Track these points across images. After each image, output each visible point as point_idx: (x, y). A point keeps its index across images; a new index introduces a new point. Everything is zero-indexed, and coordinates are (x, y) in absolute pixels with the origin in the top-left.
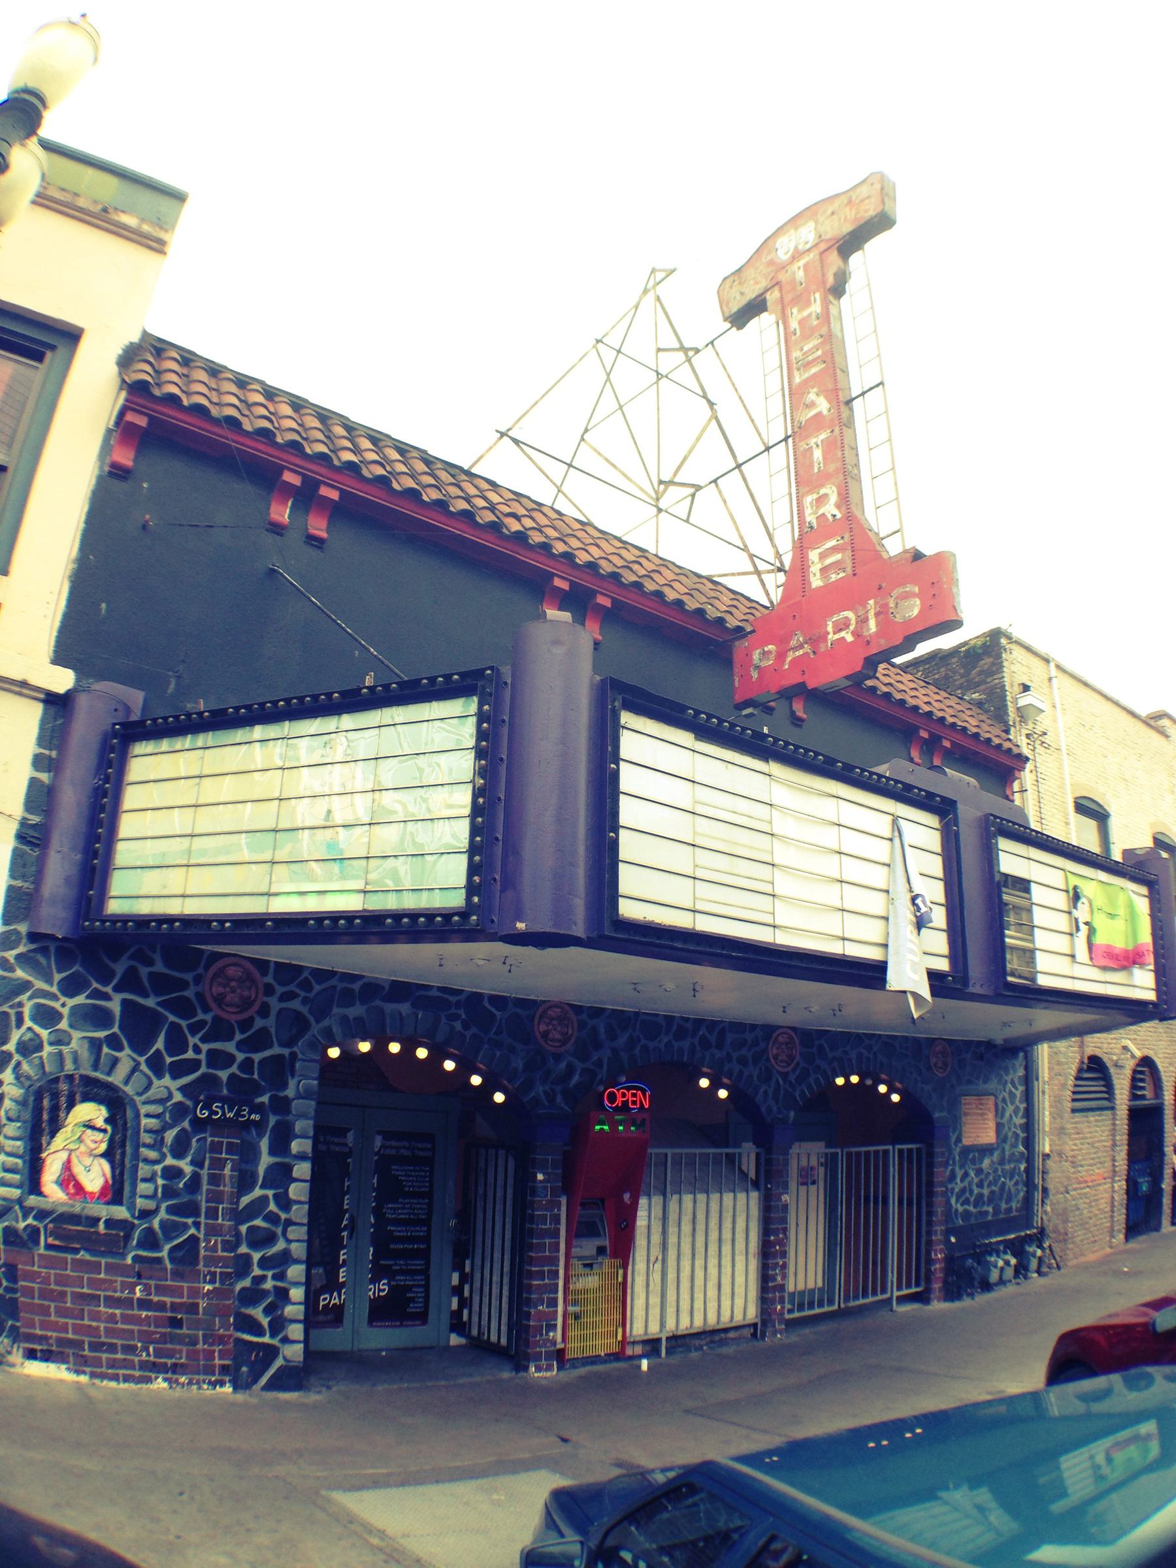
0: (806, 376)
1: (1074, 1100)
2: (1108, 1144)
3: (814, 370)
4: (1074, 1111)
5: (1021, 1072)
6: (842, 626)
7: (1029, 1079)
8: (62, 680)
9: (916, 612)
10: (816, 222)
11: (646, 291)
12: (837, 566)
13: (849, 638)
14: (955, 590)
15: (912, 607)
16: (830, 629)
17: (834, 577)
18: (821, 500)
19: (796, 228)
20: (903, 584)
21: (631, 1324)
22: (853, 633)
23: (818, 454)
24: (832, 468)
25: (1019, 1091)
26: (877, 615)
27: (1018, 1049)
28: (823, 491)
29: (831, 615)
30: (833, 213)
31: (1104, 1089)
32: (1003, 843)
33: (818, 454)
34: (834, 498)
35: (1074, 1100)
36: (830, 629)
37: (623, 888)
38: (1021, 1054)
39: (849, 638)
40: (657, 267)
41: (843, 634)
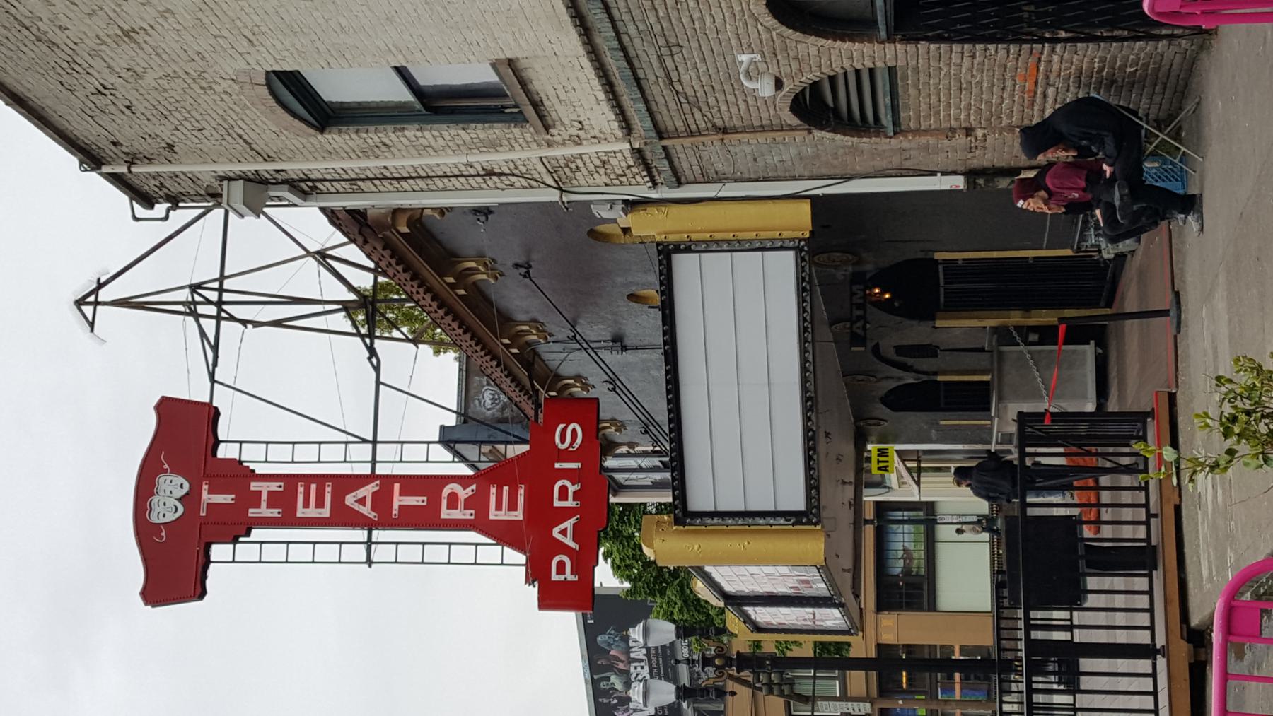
13: (577, 487)
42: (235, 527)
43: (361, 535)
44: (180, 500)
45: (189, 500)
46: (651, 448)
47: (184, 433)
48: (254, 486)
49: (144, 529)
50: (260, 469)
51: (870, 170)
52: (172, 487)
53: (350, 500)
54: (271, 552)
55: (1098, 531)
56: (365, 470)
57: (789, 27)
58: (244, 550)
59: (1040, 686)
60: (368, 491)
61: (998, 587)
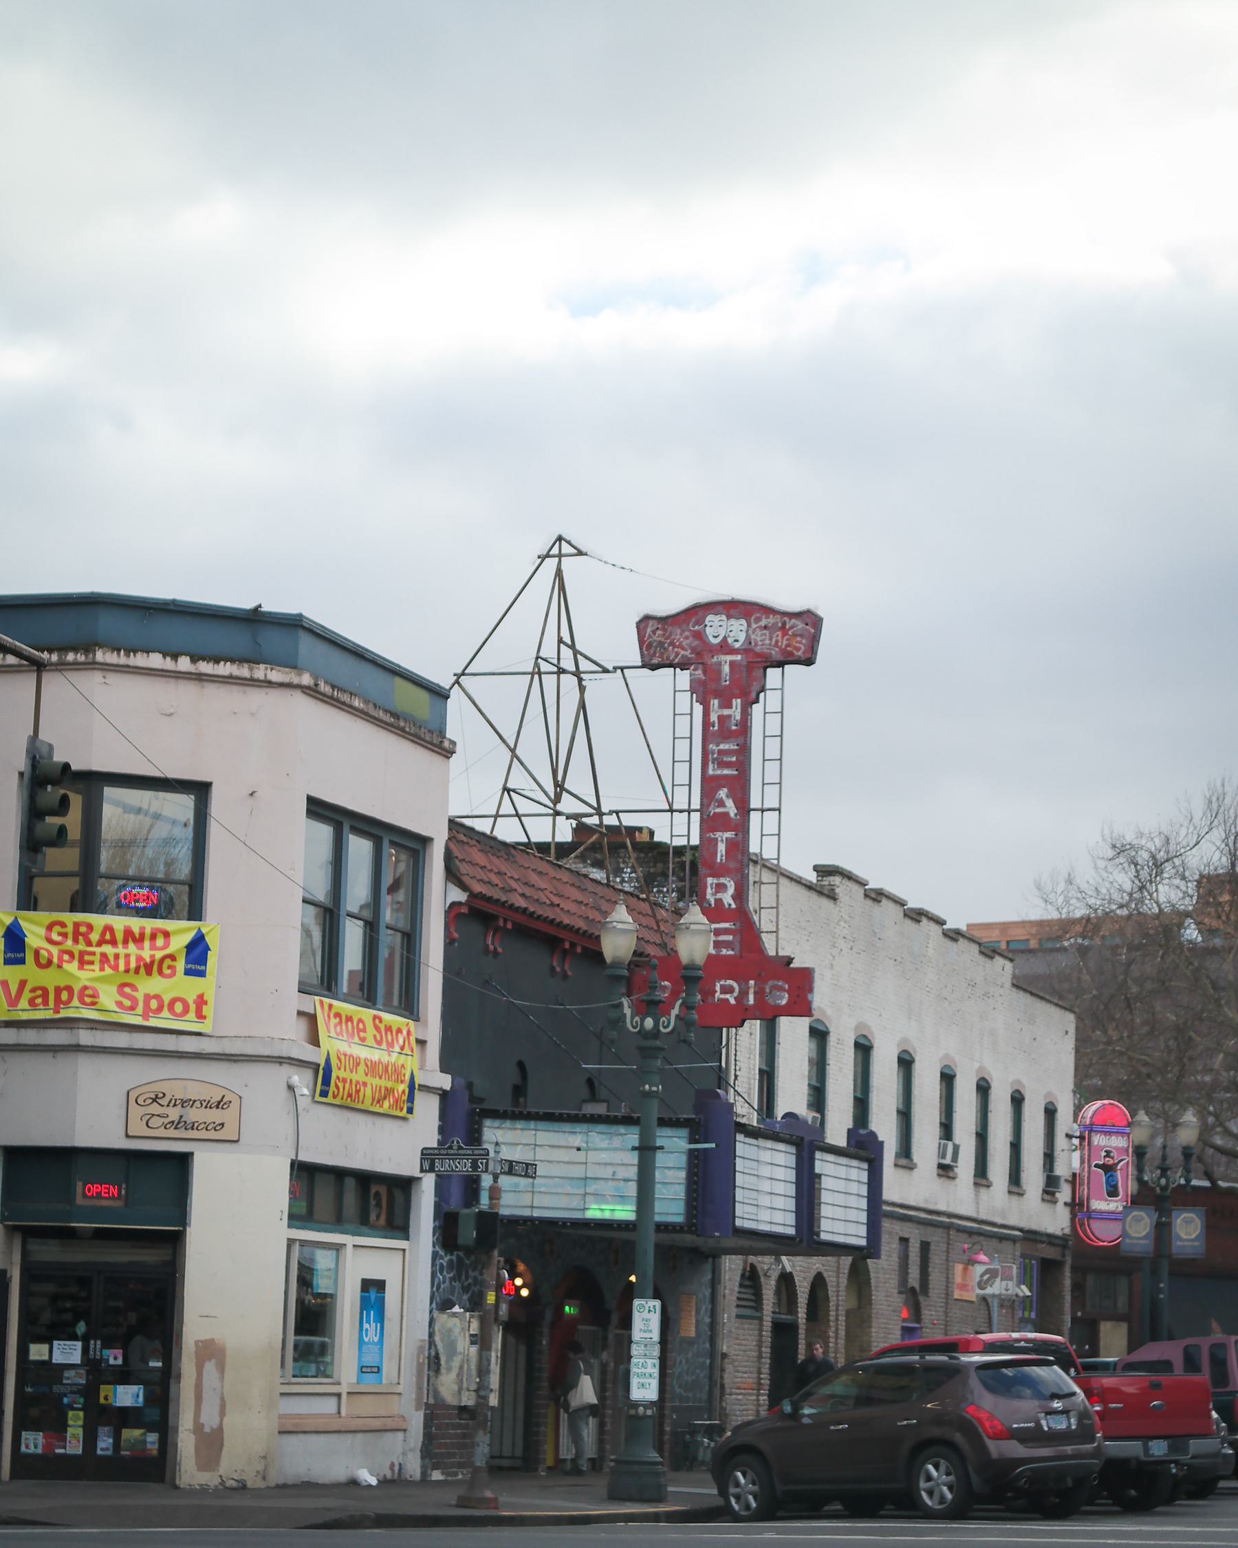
0: (719, 772)
1: (738, 1306)
2: (756, 1354)
3: (726, 772)
4: (738, 1316)
5: (709, 1277)
6: (727, 990)
7: (715, 1282)
8: (445, 1082)
9: (784, 1002)
10: (749, 625)
11: (543, 558)
12: (727, 945)
13: (733, 1001)
14: (809, 997)
15: (782, 998)
16: (718, 988)
17: (724, 952)
18: (720, 888)
19: (729, 617)
20: (778, 979)
21: (938, 1213)
22: (736, 999)
23: (722, 848)
24: (732, 865)
25: (708, 1293)
26: (755, 993)
27: (714, 1256)
28: (722, 880)
29: (720, 979)
30: (765, 627)
31: (752, 1304)
32: (818, 1155)
33: (722, 848)
34: (731, 890)
35: (738, 1306)
36: (718, 988)
37: (865, 1227)
38: (710, 1260)
39: (733, 1001)
40: (564, 536)
41: (728, 996)
42: (703, 691)
43: (696, 804)
44: (725, 639)
45: (724, 647)
46: (668, 1429)
47: (794, 638)
48: (737, 703)
49: (698, 612)
50: (757, 709)
51: (321, 1521)
52: (737, 631)
53: (723, 793)
54: (683, 722)
55: (614, 1173)
56: (755, 802)
57: (771, 1368)
58: (684, 700)
59: (92, 1346)
60: (731, 808)
61: (441, 1130)
